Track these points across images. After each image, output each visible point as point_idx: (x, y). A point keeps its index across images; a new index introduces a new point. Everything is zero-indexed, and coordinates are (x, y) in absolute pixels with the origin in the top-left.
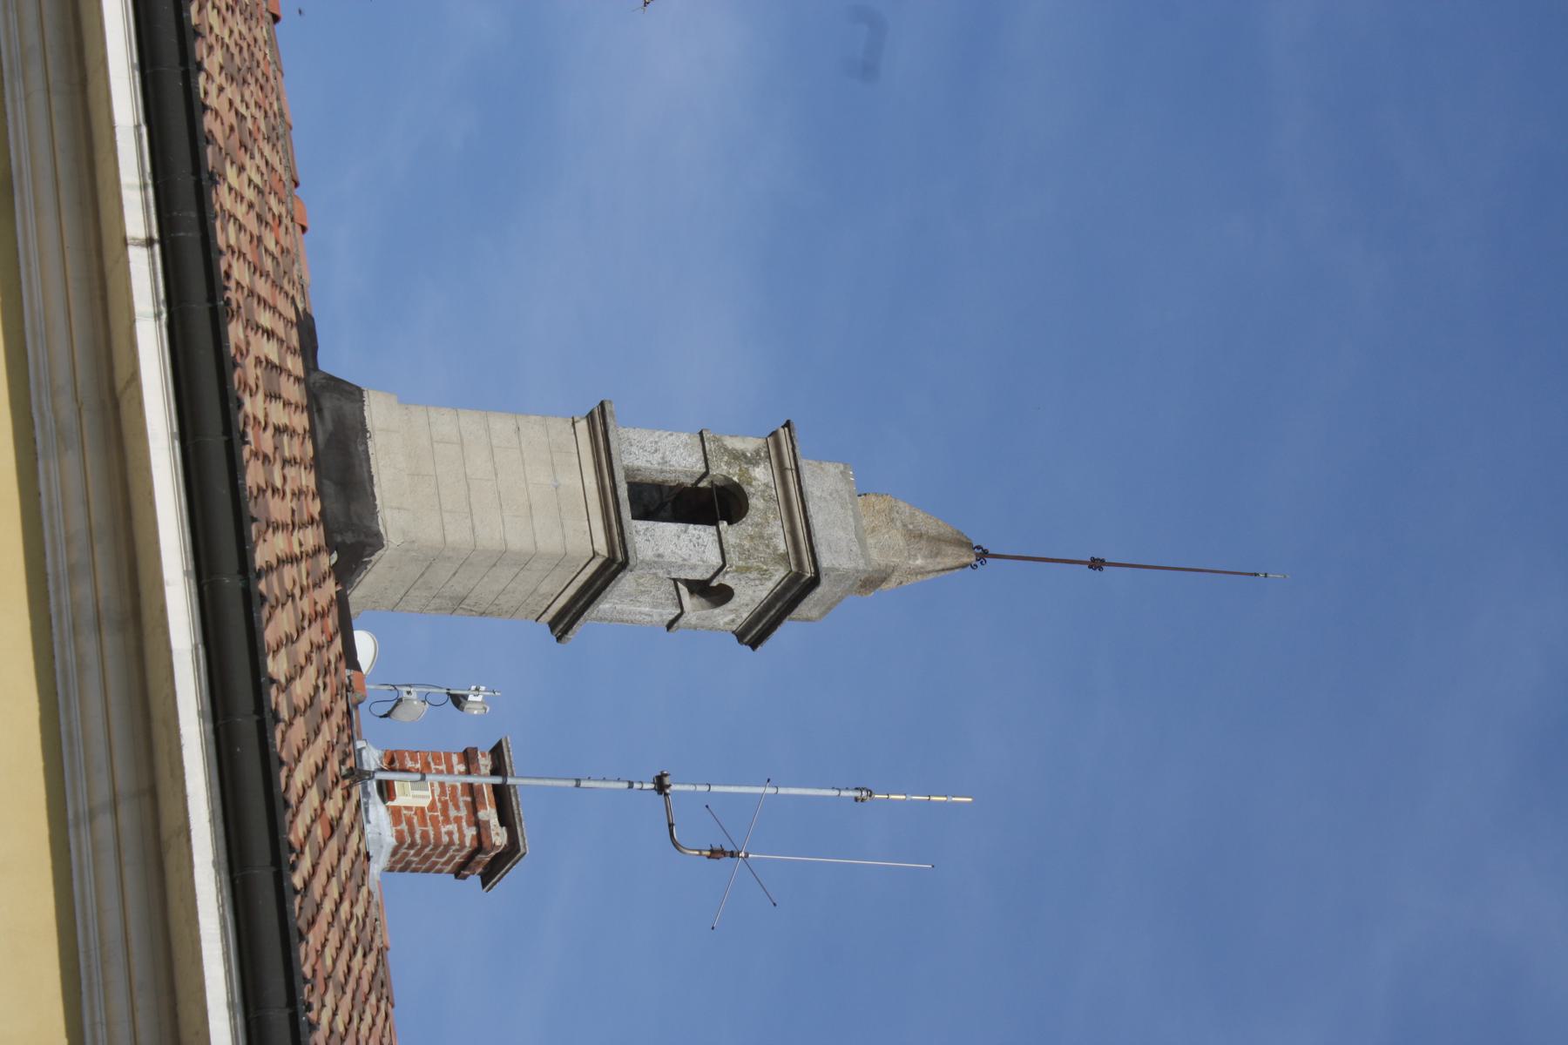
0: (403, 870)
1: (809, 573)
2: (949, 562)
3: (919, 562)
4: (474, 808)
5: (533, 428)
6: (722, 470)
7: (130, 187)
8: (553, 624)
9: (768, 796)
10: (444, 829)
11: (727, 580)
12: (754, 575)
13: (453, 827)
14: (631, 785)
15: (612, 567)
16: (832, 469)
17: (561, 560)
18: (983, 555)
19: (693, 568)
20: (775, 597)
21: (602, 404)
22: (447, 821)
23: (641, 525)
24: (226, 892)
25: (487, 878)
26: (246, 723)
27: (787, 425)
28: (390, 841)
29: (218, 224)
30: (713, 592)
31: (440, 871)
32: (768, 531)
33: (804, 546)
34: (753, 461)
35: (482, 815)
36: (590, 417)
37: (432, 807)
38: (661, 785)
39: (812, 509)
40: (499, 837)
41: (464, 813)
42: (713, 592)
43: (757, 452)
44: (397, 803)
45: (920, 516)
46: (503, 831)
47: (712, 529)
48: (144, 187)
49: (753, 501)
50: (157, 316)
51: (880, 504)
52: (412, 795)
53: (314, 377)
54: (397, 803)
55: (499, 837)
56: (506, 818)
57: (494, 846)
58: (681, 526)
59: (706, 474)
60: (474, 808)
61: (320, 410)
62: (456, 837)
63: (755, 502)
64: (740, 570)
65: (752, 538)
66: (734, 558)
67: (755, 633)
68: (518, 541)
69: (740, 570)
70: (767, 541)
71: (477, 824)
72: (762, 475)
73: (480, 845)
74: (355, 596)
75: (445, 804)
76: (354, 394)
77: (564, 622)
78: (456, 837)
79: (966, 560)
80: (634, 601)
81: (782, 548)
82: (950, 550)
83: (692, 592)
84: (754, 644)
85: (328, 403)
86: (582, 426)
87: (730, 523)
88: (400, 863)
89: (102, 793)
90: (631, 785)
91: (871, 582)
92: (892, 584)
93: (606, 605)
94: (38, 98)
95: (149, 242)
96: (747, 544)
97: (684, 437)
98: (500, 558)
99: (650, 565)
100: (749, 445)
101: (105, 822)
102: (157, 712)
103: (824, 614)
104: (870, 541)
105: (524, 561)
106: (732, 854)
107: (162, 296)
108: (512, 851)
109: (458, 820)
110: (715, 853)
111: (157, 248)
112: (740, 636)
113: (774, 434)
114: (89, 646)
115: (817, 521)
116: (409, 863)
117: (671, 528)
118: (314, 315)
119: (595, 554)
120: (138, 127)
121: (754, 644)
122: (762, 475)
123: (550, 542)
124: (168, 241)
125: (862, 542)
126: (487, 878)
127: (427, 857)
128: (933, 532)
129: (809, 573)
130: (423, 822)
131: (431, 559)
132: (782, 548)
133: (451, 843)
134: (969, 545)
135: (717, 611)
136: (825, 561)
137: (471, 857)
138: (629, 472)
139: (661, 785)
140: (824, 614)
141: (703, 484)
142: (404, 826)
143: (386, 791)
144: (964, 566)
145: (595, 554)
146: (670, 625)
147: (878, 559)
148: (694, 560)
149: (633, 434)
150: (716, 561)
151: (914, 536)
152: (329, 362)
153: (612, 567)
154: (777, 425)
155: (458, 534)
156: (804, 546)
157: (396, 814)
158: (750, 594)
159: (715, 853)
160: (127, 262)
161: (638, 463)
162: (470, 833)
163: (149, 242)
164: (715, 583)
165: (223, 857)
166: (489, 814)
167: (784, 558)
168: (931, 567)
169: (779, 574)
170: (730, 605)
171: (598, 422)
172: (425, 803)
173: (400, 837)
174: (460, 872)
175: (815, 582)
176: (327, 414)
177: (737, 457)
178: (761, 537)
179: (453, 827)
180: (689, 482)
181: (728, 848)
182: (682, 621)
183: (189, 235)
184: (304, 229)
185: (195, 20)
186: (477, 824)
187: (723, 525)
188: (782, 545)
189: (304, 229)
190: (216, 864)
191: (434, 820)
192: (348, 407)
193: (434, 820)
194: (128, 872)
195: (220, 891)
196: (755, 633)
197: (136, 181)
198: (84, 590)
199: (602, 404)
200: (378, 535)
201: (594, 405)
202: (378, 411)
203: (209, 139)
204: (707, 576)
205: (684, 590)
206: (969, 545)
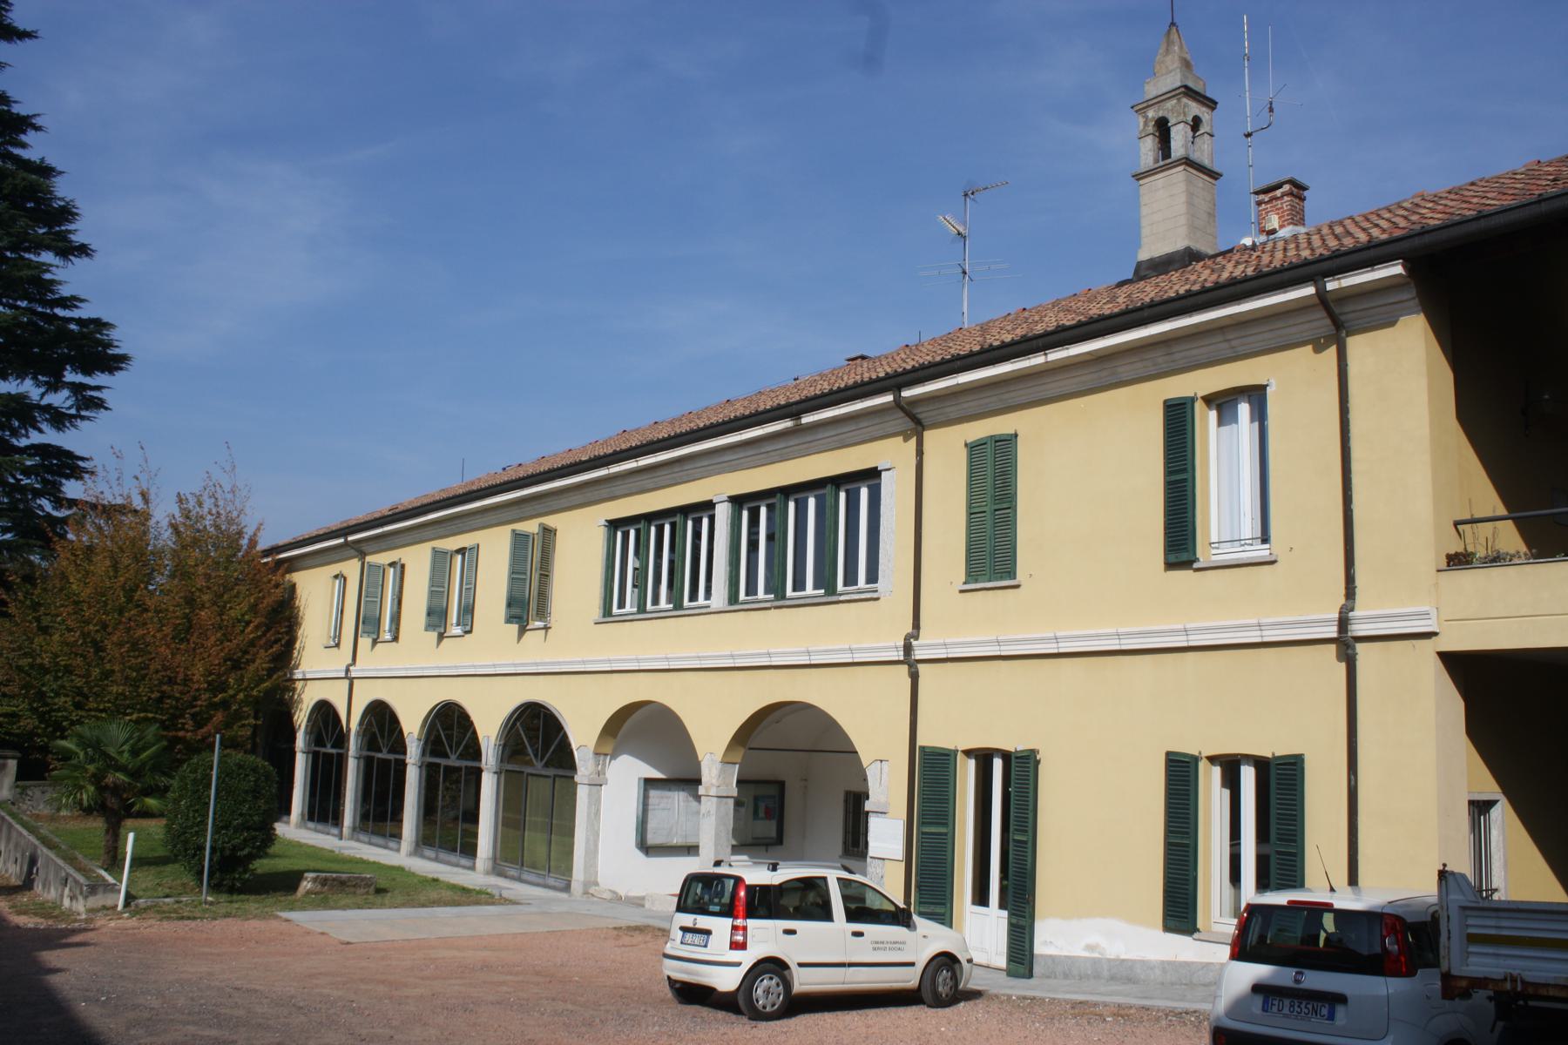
0: (1304, 220)
1: (1183, 90)
2: (1176, 36)
3: (1176, 48)
4: (1277, 198)
5: (1144, 199)
6: (1150, 129)
7: (1340, 284)
8: (1216, 179)
9: (1250, 94)
10: (1285, 208)
11: (1190, 119)
12: (1186, 109)
13: (1284, 205)
14: (1250, 146)
15: (1188, 162)
16: (1147, 87)
17: (1189, 182)
18: (1173, 24)
19: (1186, 133)
20: (1195, 100)
21: (1133, 176)
22: (1282, 208)
23: (1173, 155)
24: (1247, 299)
25: (1304, 188)
26: (1192, 301)
27: (1132, 108)
28: (1291, 227)
29: (791, 401)
30: (1196, 124)
31: (1303, 207)
32: (1170, 108)
33: (1173, 93)
34: (1146, 117)
35: (1279, 195)
36: (1138, 180)
37: (1278, 214)
38: (1248, 135)
39: (1160, 93)
40: (1286, 187)
41: (1279, 202)
42: (1196, 124)
43: (1144, 117)
44: (1277, 228)
45: (1161, 51)
46: (1284, 186)
47: (1172, 128)
48: (1029, 358)
49: (1160, 115)
50: (1067, 349)
51: (1158, 67)
52: (1274, 221)
53: (1135, 279)
54: (1277, 228)
55: (1286, 187)
56: (1279, 186)
57: (1290, 189)
58: (1172, 140)
59: (1153, 134)
60: (1277, 198)
61: (1145, 276)
62: (1287, 203)
63: (1161, 114)
64: (1185, 115)
65: (1173, 113)
66: (1181, 118)
67: (1211, 104)
68: (1183, 198)
69: (1185, 115)
70: (1173, 107)
71: (1282, 196)
72: (1151, 114)
73: (1290, 194)
74: (1211, 252)
75: (1277, 209)
76: (1139, 265)
77: (1214, 175)
78: (1287, 203)
79: (1175, 30)
80: (1204, 151)
81: (1175, 101)
82: (1172, 37)
83: (1198, 130)
84: (1216, 103)
85: (1143, 273)
86: (1141, 182)
87: (1168, 122)
88: (1301, 222)
89: (1225, 345)
90: (1250, 146)
91: (1186, 65)
92: (1188, 57)
93: (1206, 162)
94: (1012, 394)
95: (1046, 354)
96: (1175, 115)
97: (1141, 144)
98: (1190, 203)
99: (1187, 149)
100: (1141, 120)
101: (1234, 343)
102: (1195, 331)
103: (1202, 80)
104: (1171, 68)
105: (1190, 194)
106: (1271, 103)
107: (1369, 269)
108: (1292, 182)
109: (1282, 204)
110: (1271, 110)
111: (1047, 352)
112: (1213, 109)
113: (1137, 111)
114: (1177, 356)
115: (1165, 90)
116: (1300, 218)
117: (1173, 144)
118: (1117, 282)
119: (1185, 170)
120: (1012, 363)
121: (1216, 103)
122: (1151, 114)
123: (1182, 187)
124: (382, 525)
125: (1171, 72)
126: (1304, 188)
127: (1297, 212)
128: (1165, 45)
129: (1183, 90)
130: (1283, 216)
131: (1192, 228)
132: (1175, 101)
133: (1290, 205)
134: (1169, 32)
135: (1204, 120)
136: (1179, 84)
137: (1296, 196)
138: (1156, 161)
139: (1248, 135)
140: (1202, 80)
141: (1157, 134)
142: (1286, 223)
143: (1273, 232)
144: (1177, 31)
145: (1185, 170)
146: (1212, 136)
147: (1177, 64)
148: (1183, 133)
149: (1142, 163)
150: (1182, 125)
151: (1167, 52)
152: (1130, 275)
153: (1188, 162)
154: (1132, 111)
155: (1183, 220)
156: (1173, 93)
157: (1281, 227)
158: (1194, 109)
159: (1271, 110)
160: (1052, 361)
161: (1152, 158)
162: (1286, 198)
163: (1046, 354)
164: (1192, 123)
165: (1237, 302)
166: (1278, 193)
167: (1179, 100)
168: (1179, 43)
169: (1185, 100)
170: (1201, 115)
171: (1139, 177)
172: (1276, 217)
173: (1289, 224)
174: (1303, 199)
175: (1186, 87)
176: (1147, 273)
177: (1146, 124)
178: (1172, 110)
179: (1284, 205)
180: (1157, 140)
181: (1269, 106)
182: (1209, 132)
183: (1040, 342)
184: (1090, 290)
185: (1053, 328)
186: (1282, 196)
187: (1169, 124)
188: (1174, 101)
189: (1090, 290)
190: (1239, 304)
191: (1282, 212)
192: (1144, 266)
193: (1282, 212)
194: (1248, 333)
195: (1247, 302)
196: (1211, 104)
197: (739, 436)
198: (1160, 360)
199: (1133, 176)
200: (1186, 249)
201: (1133, 179)
202: (1144, 255)
203: (1013, 339)
204: (1189, 127)
205: (1197, 134)
206: (1169, 32)
